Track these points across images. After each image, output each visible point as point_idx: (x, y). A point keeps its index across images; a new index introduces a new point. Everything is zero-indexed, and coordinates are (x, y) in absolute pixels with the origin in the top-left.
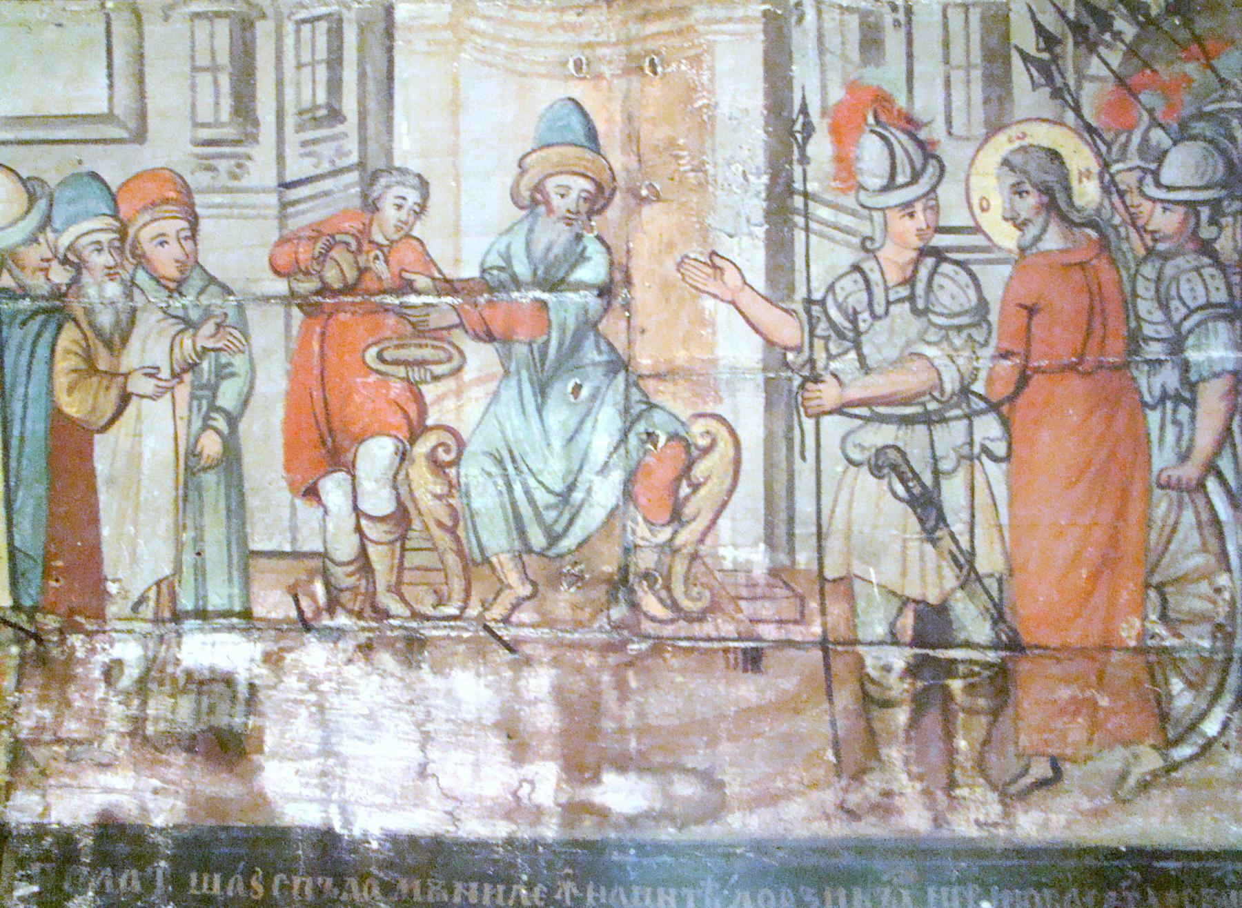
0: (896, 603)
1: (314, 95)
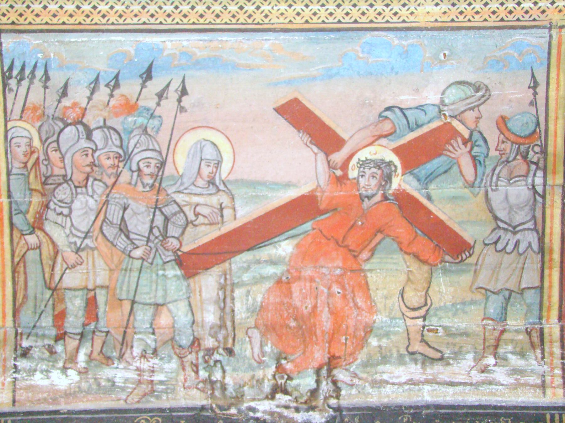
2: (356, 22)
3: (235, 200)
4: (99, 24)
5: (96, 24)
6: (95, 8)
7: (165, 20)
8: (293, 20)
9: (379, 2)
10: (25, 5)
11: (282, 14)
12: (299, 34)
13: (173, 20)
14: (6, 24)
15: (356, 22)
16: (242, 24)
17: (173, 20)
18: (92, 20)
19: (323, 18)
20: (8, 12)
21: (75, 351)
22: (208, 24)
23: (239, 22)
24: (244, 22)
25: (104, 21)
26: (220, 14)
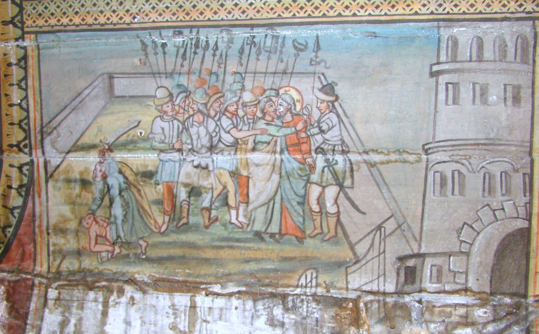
0: (501, 208)
1: (157, 83)
2: (340, 15)
3: (149, 56)
4: (225, 20)
5: (251, 19)
6: (208, 6)
7: (171, 18)
8: (326, 13)
9: (215, 3)
10: (69, 18)
11: (272, 9)
12: (335, 26)
13: (444, 10)
14: (409, 15)
15: (340, 15)
16: (512, 13)
17: (444, 10)
18: (178, 18)
19: (309, 12)
20: (164, 12)
21: (352, 123)
22: (477, 14)
23: (179, 19)
24: (514, 11)
25: (243, 17)
26: (218, 11)
